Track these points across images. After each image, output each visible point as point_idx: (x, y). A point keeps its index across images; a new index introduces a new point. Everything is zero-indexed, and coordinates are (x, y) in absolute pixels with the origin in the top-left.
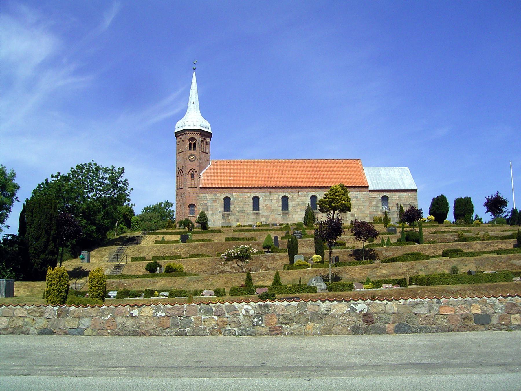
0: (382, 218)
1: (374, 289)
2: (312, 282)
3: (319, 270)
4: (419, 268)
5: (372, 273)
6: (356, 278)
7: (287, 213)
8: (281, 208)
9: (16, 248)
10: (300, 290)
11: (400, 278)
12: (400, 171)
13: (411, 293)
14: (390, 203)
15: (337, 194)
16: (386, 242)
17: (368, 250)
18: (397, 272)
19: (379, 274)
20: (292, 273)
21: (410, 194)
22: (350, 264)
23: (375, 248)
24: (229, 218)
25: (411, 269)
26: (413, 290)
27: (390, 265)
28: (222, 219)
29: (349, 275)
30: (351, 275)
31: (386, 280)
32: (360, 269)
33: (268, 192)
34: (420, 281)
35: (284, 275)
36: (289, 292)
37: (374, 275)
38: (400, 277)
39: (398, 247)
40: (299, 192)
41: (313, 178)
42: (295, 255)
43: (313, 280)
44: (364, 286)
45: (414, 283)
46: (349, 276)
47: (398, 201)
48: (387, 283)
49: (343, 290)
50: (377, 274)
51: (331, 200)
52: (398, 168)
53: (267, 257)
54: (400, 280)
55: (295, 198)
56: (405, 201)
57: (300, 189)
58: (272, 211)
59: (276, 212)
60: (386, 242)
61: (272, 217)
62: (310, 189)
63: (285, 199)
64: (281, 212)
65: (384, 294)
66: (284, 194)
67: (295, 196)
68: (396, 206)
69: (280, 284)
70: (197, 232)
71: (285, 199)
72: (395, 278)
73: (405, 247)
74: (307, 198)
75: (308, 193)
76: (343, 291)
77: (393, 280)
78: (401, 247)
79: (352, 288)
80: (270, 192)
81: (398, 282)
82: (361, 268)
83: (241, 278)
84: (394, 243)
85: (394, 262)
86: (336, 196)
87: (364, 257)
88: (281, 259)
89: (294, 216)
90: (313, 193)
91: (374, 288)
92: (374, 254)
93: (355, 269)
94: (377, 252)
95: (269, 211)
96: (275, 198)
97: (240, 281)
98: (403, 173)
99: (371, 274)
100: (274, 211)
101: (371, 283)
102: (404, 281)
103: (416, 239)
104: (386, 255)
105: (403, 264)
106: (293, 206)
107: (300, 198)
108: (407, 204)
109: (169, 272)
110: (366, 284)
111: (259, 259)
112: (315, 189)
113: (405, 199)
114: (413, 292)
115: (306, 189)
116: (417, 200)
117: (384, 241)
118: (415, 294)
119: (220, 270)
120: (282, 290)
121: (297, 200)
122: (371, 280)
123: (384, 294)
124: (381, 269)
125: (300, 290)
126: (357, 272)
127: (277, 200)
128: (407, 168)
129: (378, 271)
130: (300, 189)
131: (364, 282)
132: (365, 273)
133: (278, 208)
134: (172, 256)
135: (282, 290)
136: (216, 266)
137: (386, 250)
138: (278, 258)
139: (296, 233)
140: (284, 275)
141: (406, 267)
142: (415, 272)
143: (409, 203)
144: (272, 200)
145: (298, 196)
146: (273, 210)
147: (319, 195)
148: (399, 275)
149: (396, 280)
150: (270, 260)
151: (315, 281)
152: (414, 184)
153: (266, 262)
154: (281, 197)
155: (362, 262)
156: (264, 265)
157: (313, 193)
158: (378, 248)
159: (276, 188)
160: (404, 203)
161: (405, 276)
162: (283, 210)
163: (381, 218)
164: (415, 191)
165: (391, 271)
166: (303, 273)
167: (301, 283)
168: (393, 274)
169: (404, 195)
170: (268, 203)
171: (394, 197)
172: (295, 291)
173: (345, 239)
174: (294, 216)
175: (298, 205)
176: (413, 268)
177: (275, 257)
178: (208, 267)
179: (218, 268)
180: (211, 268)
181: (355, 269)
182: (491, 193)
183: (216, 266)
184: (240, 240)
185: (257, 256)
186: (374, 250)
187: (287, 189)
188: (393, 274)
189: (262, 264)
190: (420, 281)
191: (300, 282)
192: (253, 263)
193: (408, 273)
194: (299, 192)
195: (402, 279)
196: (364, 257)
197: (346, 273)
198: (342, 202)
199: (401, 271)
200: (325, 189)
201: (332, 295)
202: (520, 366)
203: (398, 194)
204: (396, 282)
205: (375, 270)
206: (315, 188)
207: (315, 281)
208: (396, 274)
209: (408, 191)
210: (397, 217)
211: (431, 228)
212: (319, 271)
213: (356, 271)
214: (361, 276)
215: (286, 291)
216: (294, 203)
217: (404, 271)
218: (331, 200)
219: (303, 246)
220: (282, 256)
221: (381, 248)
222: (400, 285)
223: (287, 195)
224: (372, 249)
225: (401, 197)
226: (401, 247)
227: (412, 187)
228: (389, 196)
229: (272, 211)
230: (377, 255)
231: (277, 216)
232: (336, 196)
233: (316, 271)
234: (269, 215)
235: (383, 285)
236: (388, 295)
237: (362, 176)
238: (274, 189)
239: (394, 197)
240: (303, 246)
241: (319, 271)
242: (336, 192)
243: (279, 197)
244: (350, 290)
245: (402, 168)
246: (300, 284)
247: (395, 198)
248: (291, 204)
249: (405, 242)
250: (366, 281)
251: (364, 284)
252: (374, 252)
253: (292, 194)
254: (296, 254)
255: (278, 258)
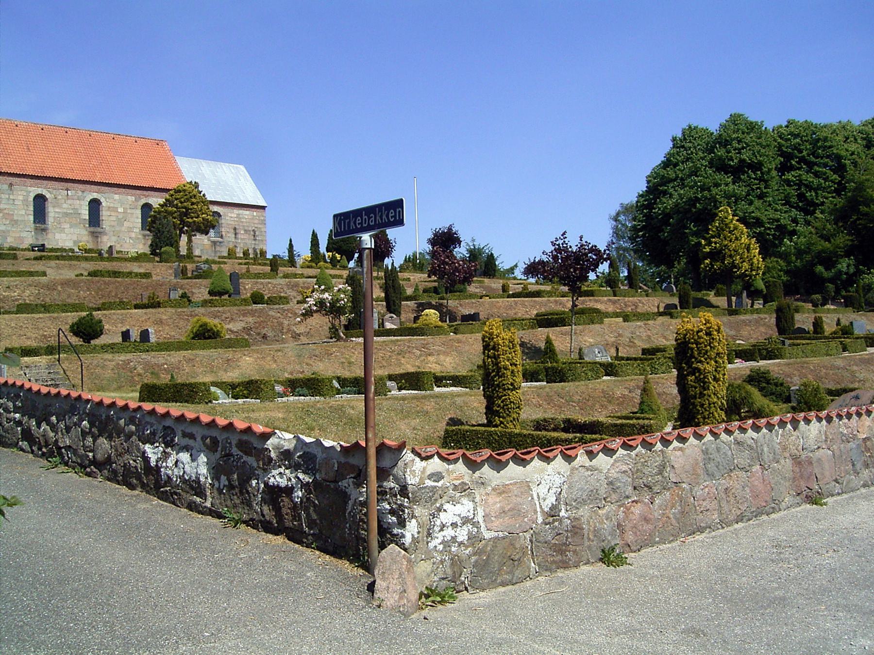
7: (44, 230)
8: (32, 218)
9: (472, 256)
12: (233, 171)
14: (223, 225)
15: (193, 200)
21: (255, 214)
33: (6, 184)
40: (67, 190)
41: (91, 165)
47: (236, 223)
51: (184, 210)
52: (227, 164)
55: (60, 201)
56: (248, 224)
57: (70, 184)
58: (15, 223)
59: (21, 226)
61: (14, 235)
62: (89, 186)
63: (40, 201)
64: (33, 226)
66: (40, 191)
67: (60, 197)
68: (233, 231)
71: (40, 201)
74: (82, 202)
75: (85, 194)
80: (11, 185)
86: (193, 204)
89: (58, 236)
90: (95, 194)
95: (8, 222)
96: (21, 198)
98: (239, 175)
100: (19, 223)
106: (57, 216)
107: (69, 202)
108: (250, 231)
109: (205, 338)
112: (99, 187)
113: (248, 220)
115: (81, 186)
116: (265, 224)
121: (65, 206)
127: (25, 201)
128: (242, 167)
130: (70, 185)
133: (26, 217)
134: (65, 305)
143: (254, 228)
144: (14, 200)
145: (66, 198)
146: (16, 222)
147: (105, 198)
152: (260, 196)
154: (32, 195)
157: (95, 195)
159: (24, 177)
160: (246, 228)
162: (34, 222)
164: (263, 208)
169: (246, 213)
170: (6, 207)
171: (230, 215)
174: (58, 236)
175: (66, 215)
182: (442, 225)
187: (45, 182)
194: (67, 190)
198: (204, 215)
200: (116, 189)
202: (873, 488)
203: (237, 211)
206: (99, 185)
207: (599, 352)
209: (253, 208)
216: (57, 210)
218: (184, 210)
223: (44, 192)
225: (241, 216)
227: (258, 201)
228: (221, 214)
229: (13, 223)
231: (24, 234)
232: (193, 204)
234: (9, 231)
237: (177, 172)
238: (19, 179)
239: (230, 215)
242: (191, 197)
243: (28, 196)
245: (235, 165)
247: (232, 217)
248: (52, 212)
253: (55, 191)
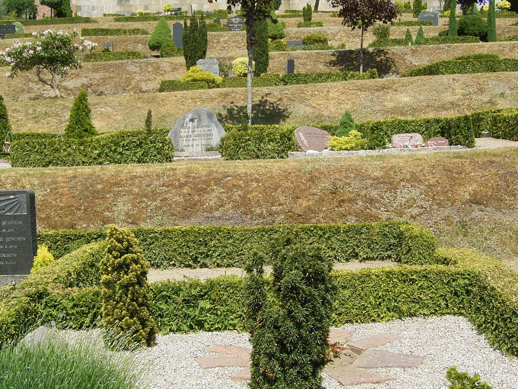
0: (411, 4)
1: (362, 152)
2: (182, 126)
3: (233, 92)
4: (498, 91)
5: (372, 101)
6: (329, 113)
10: (115, 151)
11: (449, 117)
13: (494, 171)
16: (414, 38)
17: (373, 53)
18: (439, 101)
19: (390, 105)
20: (163, 100)
22: (319, 78)
23: (389, 48)
24: (131, 4)
25: (475, 93)
26: (497, 159)
27: (420, 82)
28: (118, 4)
29: (310, 105)
30: (314, 107)
31: (406, 122)
32: (342, 90)
34: (506, 127)
35: (139, 105)
36: (79, 158)
37: (377, 108)
38: (445, 112)
39: (441, 45)
42: (199, 58)
43: (187, 120)
44: (332, 140)
45: (485, 132)
46: (309, 110)
48: (407, 132)
49: (259, 153)
50: (386, 103)
53: (142, 65)
54: (448, 122)
60: (414, 38)
65: (391, 173)
69: (86, 130)
70: (45, 22)
72: (431, 116)
73: (457, 47)
76: (258, 157)
77: (428, 122)
78: (450, 47)
79: (290, 148)
81: (443, 128)
82: (344, 87)
83: (31, 111)
84: (432, 39)
85: (430, 74)
87: (361, 67)
88: (174, 69)
91: (363, 148)
92: (387, 60)
93: (328, 92)
94: (394, 57)
97: (24, 119)
99: (369, 104)
101: (354, 132)
102: (462, 124)
103: (480, 33)
104: (414, 63)
105: (454, 79)
110: (340, 135)
111: (125, 70)
114: (500, 166)
117: (411, 36)
118: (504, 176)
119: (33, 95)
120: (57, 150)
122: (357, 122)
123: (391, 173)
124: (396, 90)
125: (115, 151)
126: (333, 98)
129: (388, 98)
131: (336, 128)
132: (354, 103)
135: (57, 150)
136: (25, 84)
137: (414, 52)
138: (168, 69)
139: (232, 23)
140: (139, 105)
141: (463, 89)
142: (486, 100)
148: (444, 107)
149: (438, 121)
150: (148, 72)
151: (192, 120)
153: (138, 78)
155: (349, 76)
156: (133, 83)
158: (395, 47)
161: (458, 111)
163: (409, 3)
165: (421, 98)
166: (190, 101)
167: (153, 128)
168: (428, 106)
172: (99, 155)
173: (329, 32)
176: (481, 91)
177: (162, 66)
178: (7, 89)
179: (30, 91)
180: (14, 90)
181: (328, 92)
183: (25, 84)
184: (111, 34)
185: (121, 63)
186: (387, 53)
188: (428, 106)
189: (128, 81)
190: (506, 127)
191: (148, 122)
192: (110, 78)
193: (467, 102)
195: (459, 119)
196: (361, 67)
197: (303, 100)
199: (448, 97)
201: (204, 173)
204: (436, 127)
205: (381, 93)
207: (192, 120)
208: (437, 104)
210: (439, 5)
211: (507, 19)
212: (233, 95)
213: (331, 95)
214: (342, 109)
215: (69, 154)
217: (457, 97)
219: (240, 45)
220: (176, 65)
221: (403, 47)
222: (449, 137)
224: (383, 50)
226: (450, 47)
230: (393, 62)
233: (227, 95)
235: (396, 138)
236: (408, 177)
240: (240, 45)
241: (233, 95)
244: (282, 154)
246: (149, 132)
249: (456, 37)
250: (342, 124)
251: (333, 134)
252: (387, 56)
254: (264, 72)
255: (168, 69)
